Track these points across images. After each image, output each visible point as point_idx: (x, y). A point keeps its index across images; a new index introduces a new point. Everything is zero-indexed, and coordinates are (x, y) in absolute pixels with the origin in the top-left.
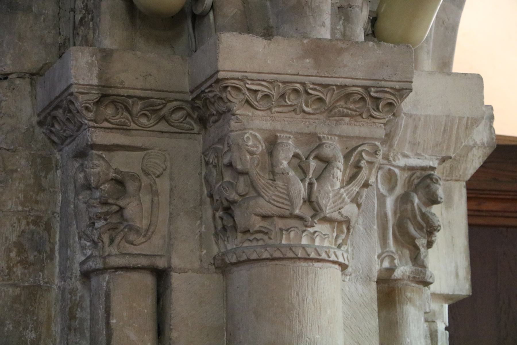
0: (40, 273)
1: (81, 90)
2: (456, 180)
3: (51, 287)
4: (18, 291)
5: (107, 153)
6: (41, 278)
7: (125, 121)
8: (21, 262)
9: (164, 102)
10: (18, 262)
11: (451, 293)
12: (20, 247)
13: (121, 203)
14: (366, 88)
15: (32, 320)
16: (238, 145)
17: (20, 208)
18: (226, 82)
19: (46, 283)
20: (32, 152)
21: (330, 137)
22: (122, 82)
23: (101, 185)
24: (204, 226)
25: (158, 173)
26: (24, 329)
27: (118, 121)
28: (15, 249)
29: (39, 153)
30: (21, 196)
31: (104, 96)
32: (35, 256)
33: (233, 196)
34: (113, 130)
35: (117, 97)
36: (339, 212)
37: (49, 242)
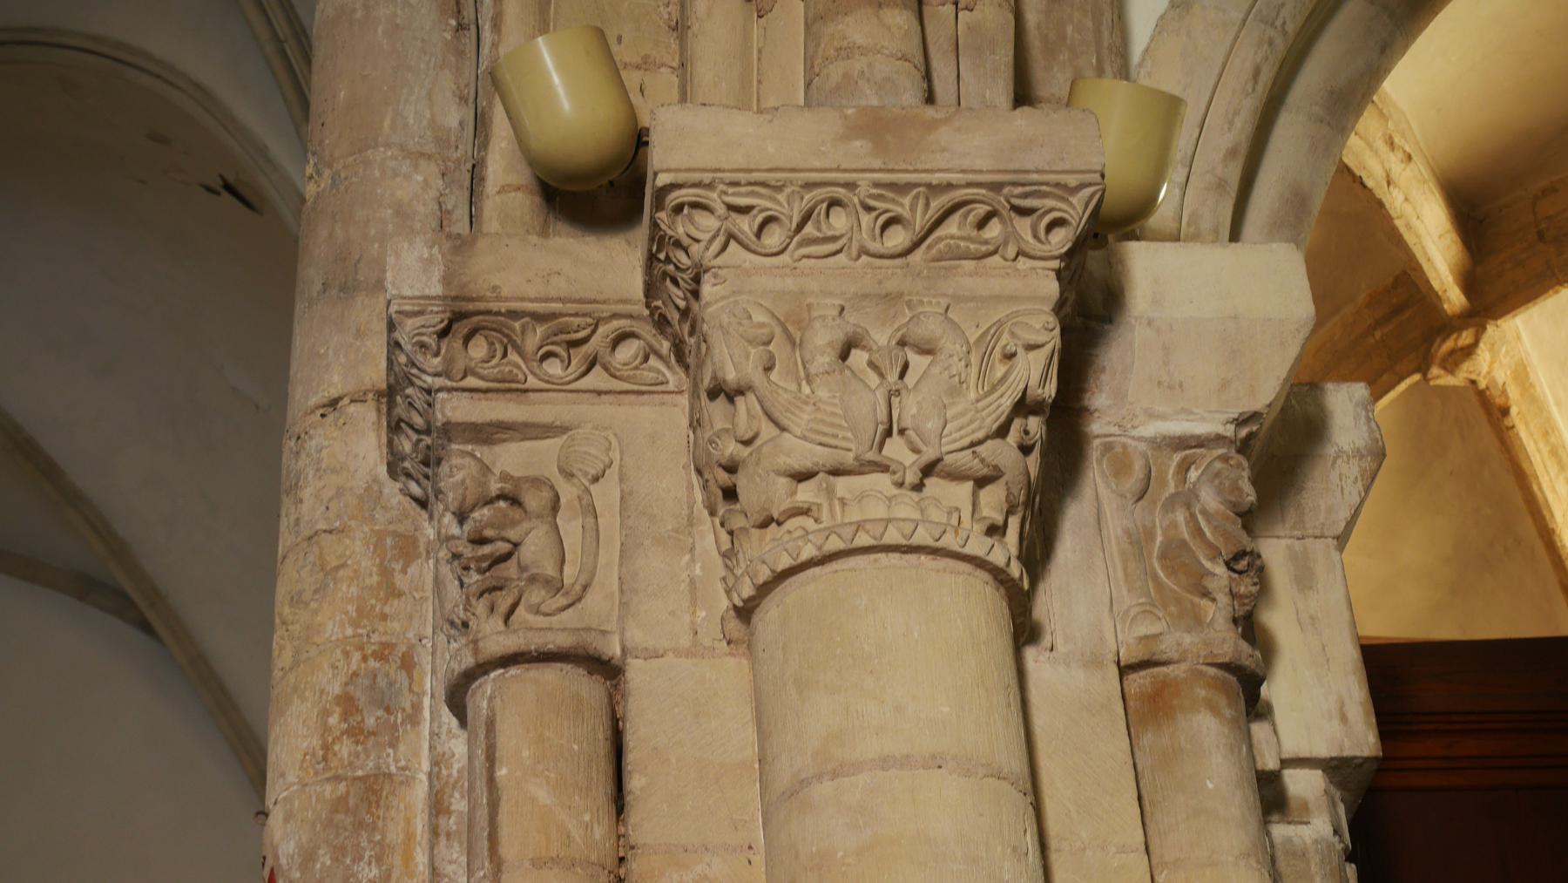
0: (391, 751)
1: (408, 308)
3: (414, 778)
4: (342, 787)
5: (485, 448)
6: (391, 760)
9: (589, 320)
10: (346, 732)
11: (1334, 754)
12: (348, 704)
13: (512, 534)
14: (996, 187)
15: (370, 841)
17: (349, 632)
22: (495, 288)
23: (472, 510)
24: (698, 565)
25: (593, 472)
26: (353, 861)
28: (338, 709)
29: (391, 527)
30: (351, 608)
31: (458, 317)
33: (731, 448)
34: (490, 395)
37: (410, 690)
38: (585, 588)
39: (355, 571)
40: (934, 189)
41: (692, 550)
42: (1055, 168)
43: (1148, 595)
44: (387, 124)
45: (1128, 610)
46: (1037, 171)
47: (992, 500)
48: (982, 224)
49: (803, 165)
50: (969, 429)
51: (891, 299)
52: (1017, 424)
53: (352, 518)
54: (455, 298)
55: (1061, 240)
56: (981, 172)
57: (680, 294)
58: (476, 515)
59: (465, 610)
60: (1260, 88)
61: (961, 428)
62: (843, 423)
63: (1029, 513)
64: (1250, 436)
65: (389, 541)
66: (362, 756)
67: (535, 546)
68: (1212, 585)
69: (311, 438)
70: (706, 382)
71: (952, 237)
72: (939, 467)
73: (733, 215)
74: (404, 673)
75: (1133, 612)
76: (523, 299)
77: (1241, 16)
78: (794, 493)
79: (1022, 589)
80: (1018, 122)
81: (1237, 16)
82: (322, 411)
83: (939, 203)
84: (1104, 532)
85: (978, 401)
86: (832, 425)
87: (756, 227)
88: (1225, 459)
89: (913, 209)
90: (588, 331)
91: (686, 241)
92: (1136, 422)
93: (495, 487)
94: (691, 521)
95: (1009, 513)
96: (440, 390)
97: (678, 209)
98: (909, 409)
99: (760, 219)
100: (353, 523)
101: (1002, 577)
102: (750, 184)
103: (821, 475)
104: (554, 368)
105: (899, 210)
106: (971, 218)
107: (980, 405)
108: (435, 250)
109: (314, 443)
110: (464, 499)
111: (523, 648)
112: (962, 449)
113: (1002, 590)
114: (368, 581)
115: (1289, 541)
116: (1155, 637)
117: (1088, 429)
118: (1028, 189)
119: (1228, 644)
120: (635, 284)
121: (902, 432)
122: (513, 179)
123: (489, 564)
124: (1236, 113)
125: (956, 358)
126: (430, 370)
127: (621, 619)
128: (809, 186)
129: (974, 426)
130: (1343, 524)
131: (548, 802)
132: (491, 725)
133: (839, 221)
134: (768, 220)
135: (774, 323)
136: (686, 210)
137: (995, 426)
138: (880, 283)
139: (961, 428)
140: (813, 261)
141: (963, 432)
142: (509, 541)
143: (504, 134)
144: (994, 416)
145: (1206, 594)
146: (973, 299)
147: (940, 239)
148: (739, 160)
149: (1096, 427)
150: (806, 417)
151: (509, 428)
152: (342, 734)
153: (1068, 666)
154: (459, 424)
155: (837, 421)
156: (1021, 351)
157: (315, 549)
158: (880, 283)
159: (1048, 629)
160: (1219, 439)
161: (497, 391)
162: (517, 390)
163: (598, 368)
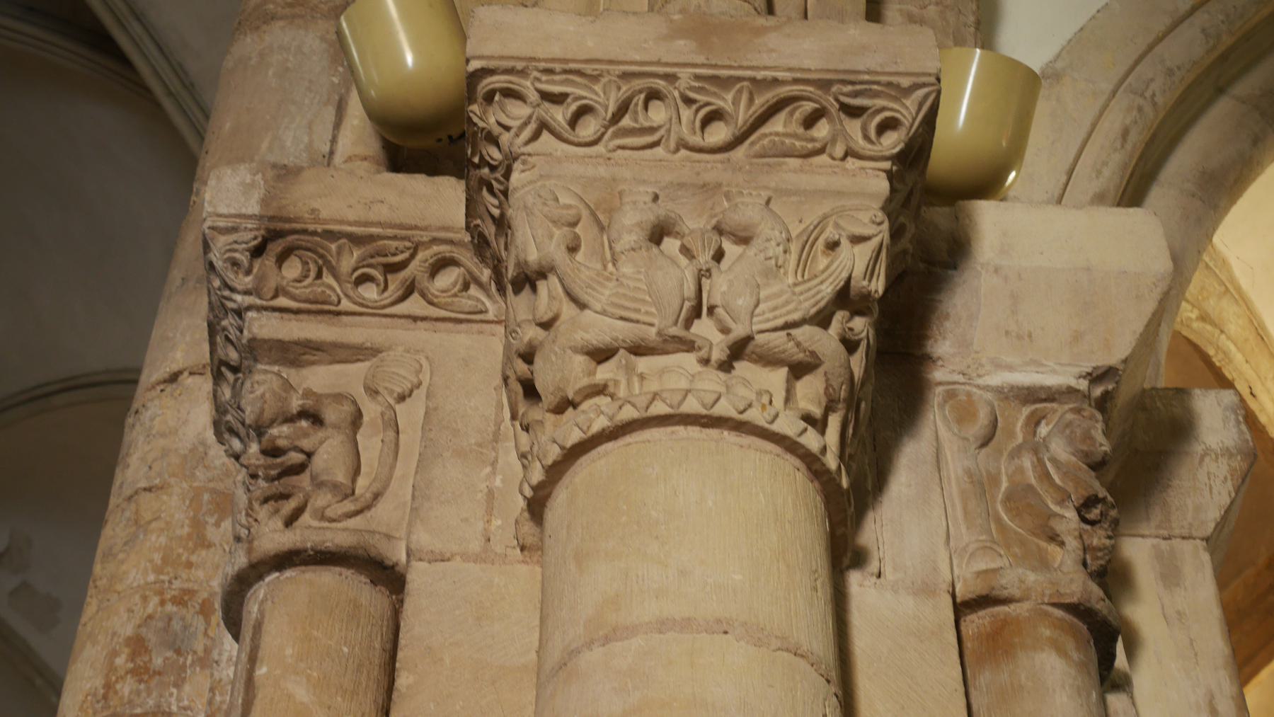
0: (174, 691)
2: (1184, 538)
5: (293, 371)
6: (173, 700)
7: (323, 292)
8: (132, 672)
9: (408, 244)
13: (306, 444)
14: (824, 85)
16: (525, 207)
17: (151, 578)
18: (485, 82)
19: (185, 709)
20: (195, 484)
21: (754, 193)
22: (313, 211)
23: (272, 423)
25: (399, 390)
27: (308, 291)
28: (127, 650)
29: (212, 485)
30: (157, 557)
31: (272, 235)
32: (167, 659)
33: (531, 333)
34: (301, 317)
35: (302, 237)
36: (789, 335)
37: (206, 634)
38: (377, 496)
39: (167, 523)
40: (759, 85)
41: (494, 464)
42: (887, 70)
43: (989, 532)
44: (265, 145)
45: (967, 545)
46: (868, 72)
47: (810, 392)
48: (810, 121)
49: (621, 58)
50: (784, 310)
51: (708, 189)
52: (840, 316)
53: (174, 475)
54: (272, 218)
55: (892, 142)
56: (809, 70)
57: (496, 202)
58: (274, 431)
59: (248, 515)
60: (1129, 146)
61: (775, 309)
62: (647, 298)
63: (852, 416)
64: (1106, 396)
65: (206, 497)
66: (144, 694)
67: (329, 454)
68: (1060, 527)
69: (147, 410)
70: (511, 272)
71: (777, 134)
72: (750, 348)
73: (547, 105)
74: (201, 617)
75: (972, 547)
76: (341, 222)
77: (1111, 87)
78: (592, 373)
79: (839, 486)
80: (852, 32)
81: (1107, 87)
82: (162, 387)
83: (763, 100)
84: (944, 473)
85: (795, 285)
86: (635, 300)
87: (569, 115)
88: (1078, 411)
89: (736, 102)
90: (406, 255)
91: (497, 130)
92: (981, 372)
93: (296, 404)
94: (496, 437)
95: (829, 409)
96: (249, 308)
97: (489, 98)
98: (719, 288)
99: (574, 107)
100: (172, 481)
101: (816, 466)
102: (565, 72)
103: (622, 352)
104: (370, 292)
105: (721, 103)
106: (797, 115)
107: (797, 289)
108: (259, 176)
109: (149, 413)
110: (262, 411)
111: (299, 545)
112: (775, 329)
113: (817, 484)
114: (178, 532)
115: (1155, 541)
116: (995, 571)
117: (930, 376)
118: (858, 87)
119: (1077, 585)
120: (458, 216)
121: (711, 310)
122: (361, 150)
123: (282, 473)
124: (1105, 164)
125: (773, 243)
126: (239, 287)
127: (410, 524)
128: (626, 76)
129: (791, 307)
130: (1212, 525)
131: (306, 700)
132: (258, 627)
133: (658, 114)
134: (584, 111)
135: (581, 206)
136: (497, 98)
137: (813, 311)
138: (698, 174)
139: (775, 309)
140: (628, 153)
141: (777, 313)
142: (302, 451)
143: (356, 122)
144: (813, 301)
145: (1054, 538)
146: (796, 193)
147: (765, 135)
148: (556, 51)
149: (938, 375)
150: (607, 292)
151: (318, 349)
152: (127, 673)
153: (896, 592)
154: (265, 341)
155: (641, 296)
156: (845, 243)
157: (133, 506)
158: (698, 174)
159: (875, 555)
160: (1071, 391)
161: (309, 312)
162: (329, 312)
163: (416, 296)
